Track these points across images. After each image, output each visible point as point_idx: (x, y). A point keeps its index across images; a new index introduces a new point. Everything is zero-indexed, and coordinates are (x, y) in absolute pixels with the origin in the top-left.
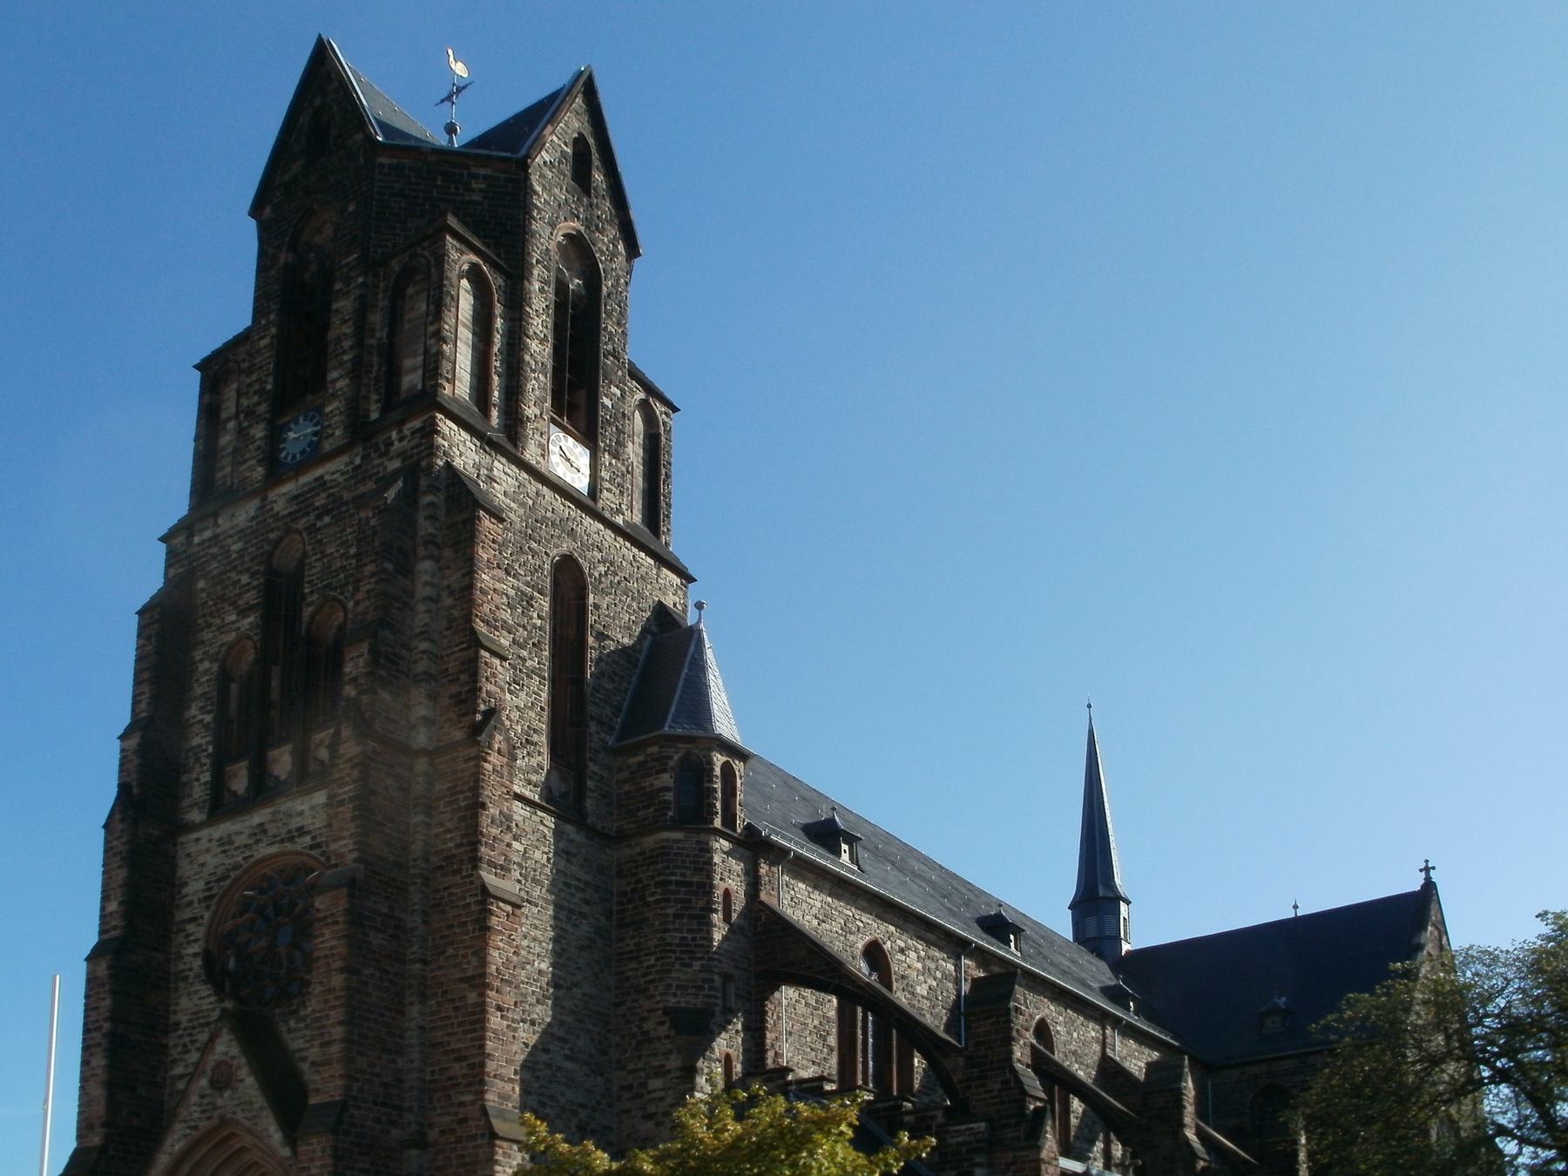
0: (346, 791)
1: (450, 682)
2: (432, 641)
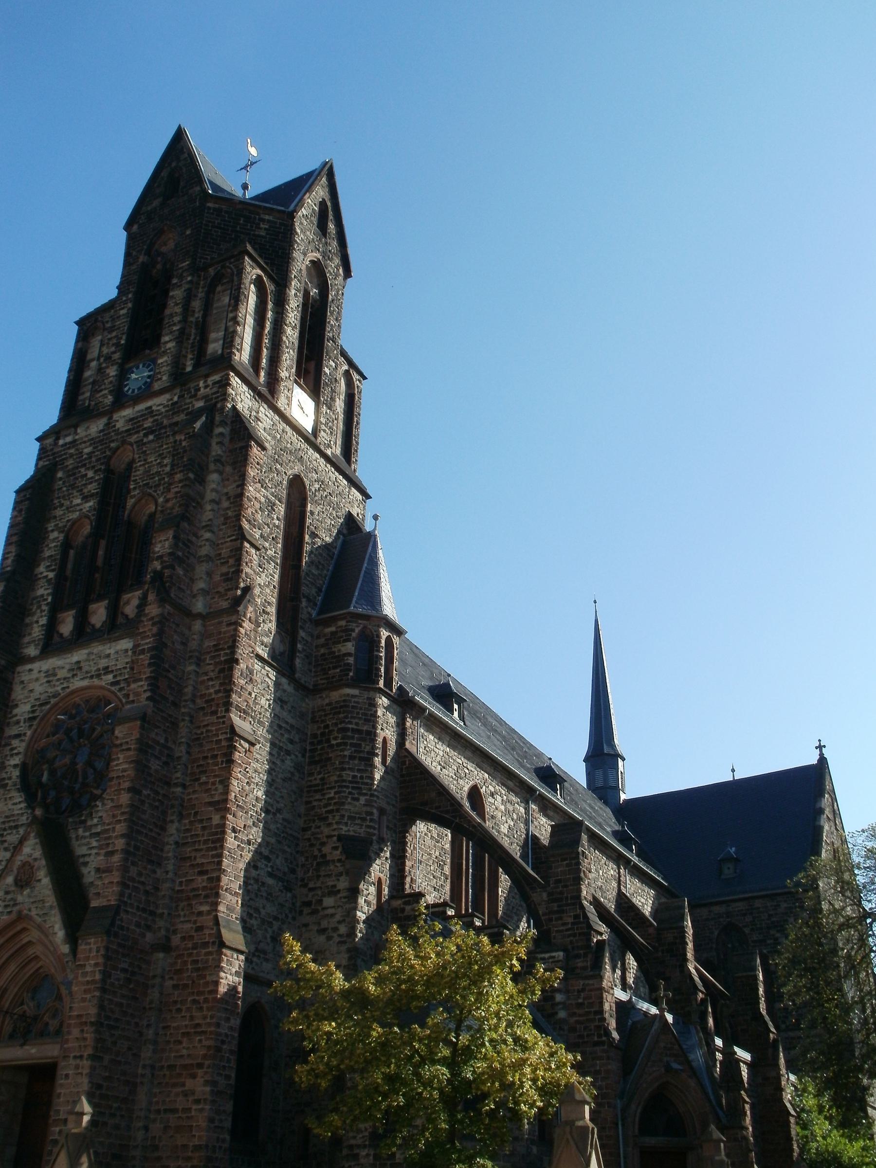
0: (148, 642)
1: (222, 563)
2: (213, 532)
